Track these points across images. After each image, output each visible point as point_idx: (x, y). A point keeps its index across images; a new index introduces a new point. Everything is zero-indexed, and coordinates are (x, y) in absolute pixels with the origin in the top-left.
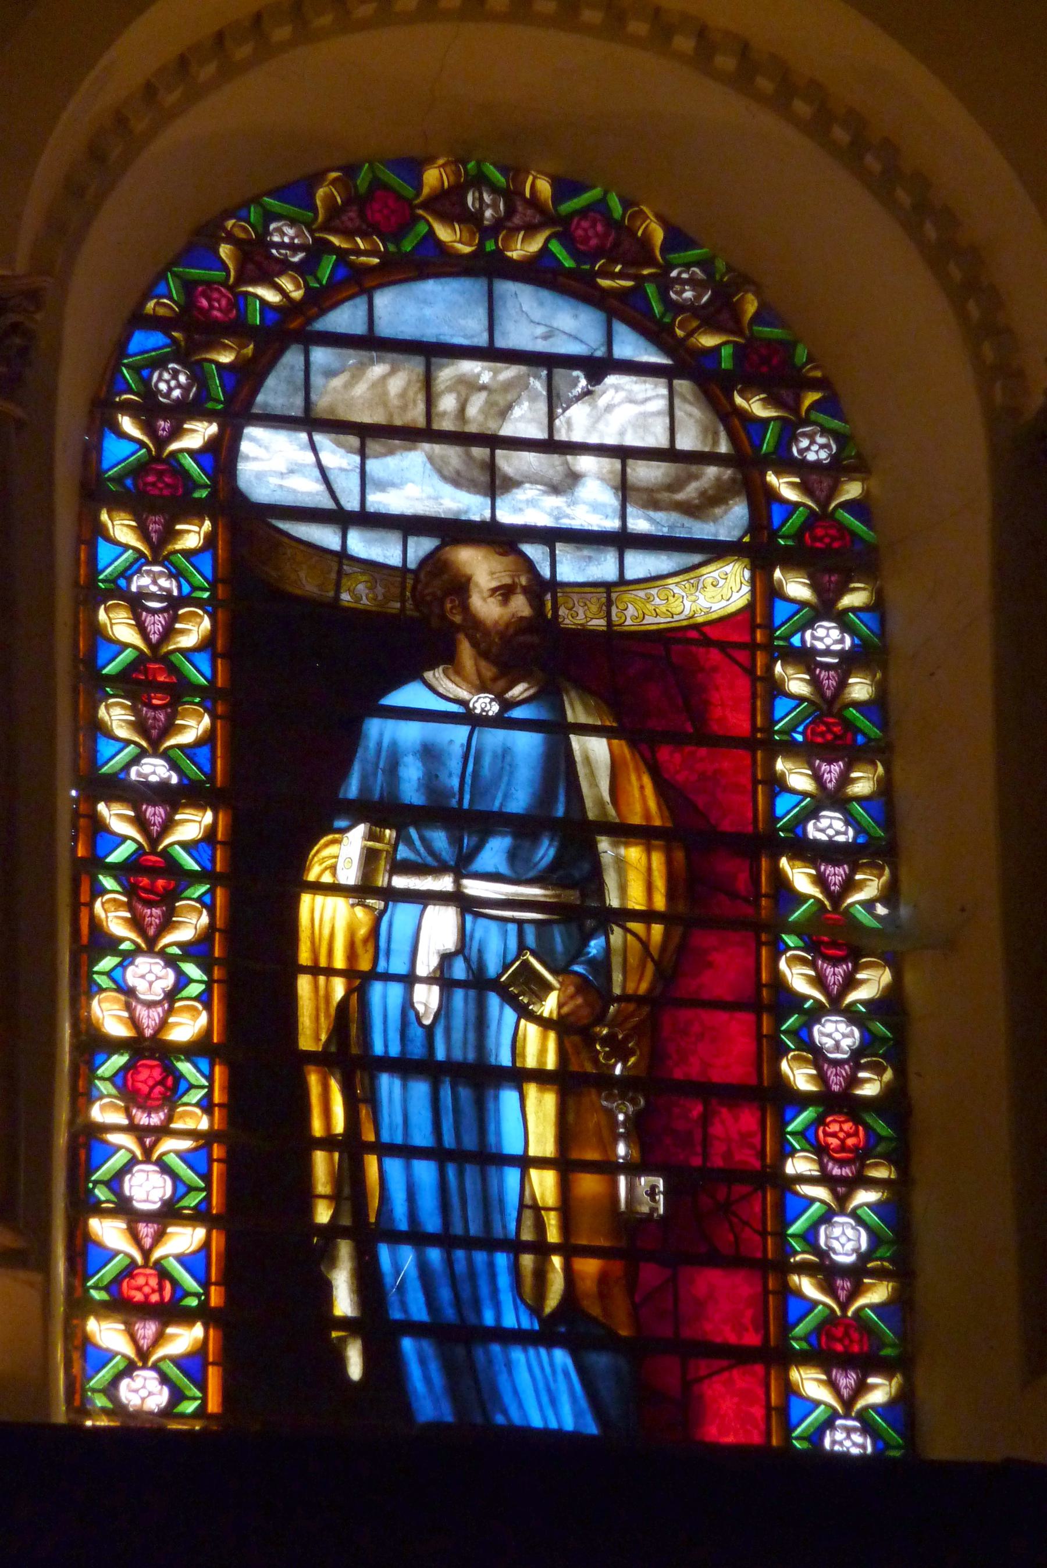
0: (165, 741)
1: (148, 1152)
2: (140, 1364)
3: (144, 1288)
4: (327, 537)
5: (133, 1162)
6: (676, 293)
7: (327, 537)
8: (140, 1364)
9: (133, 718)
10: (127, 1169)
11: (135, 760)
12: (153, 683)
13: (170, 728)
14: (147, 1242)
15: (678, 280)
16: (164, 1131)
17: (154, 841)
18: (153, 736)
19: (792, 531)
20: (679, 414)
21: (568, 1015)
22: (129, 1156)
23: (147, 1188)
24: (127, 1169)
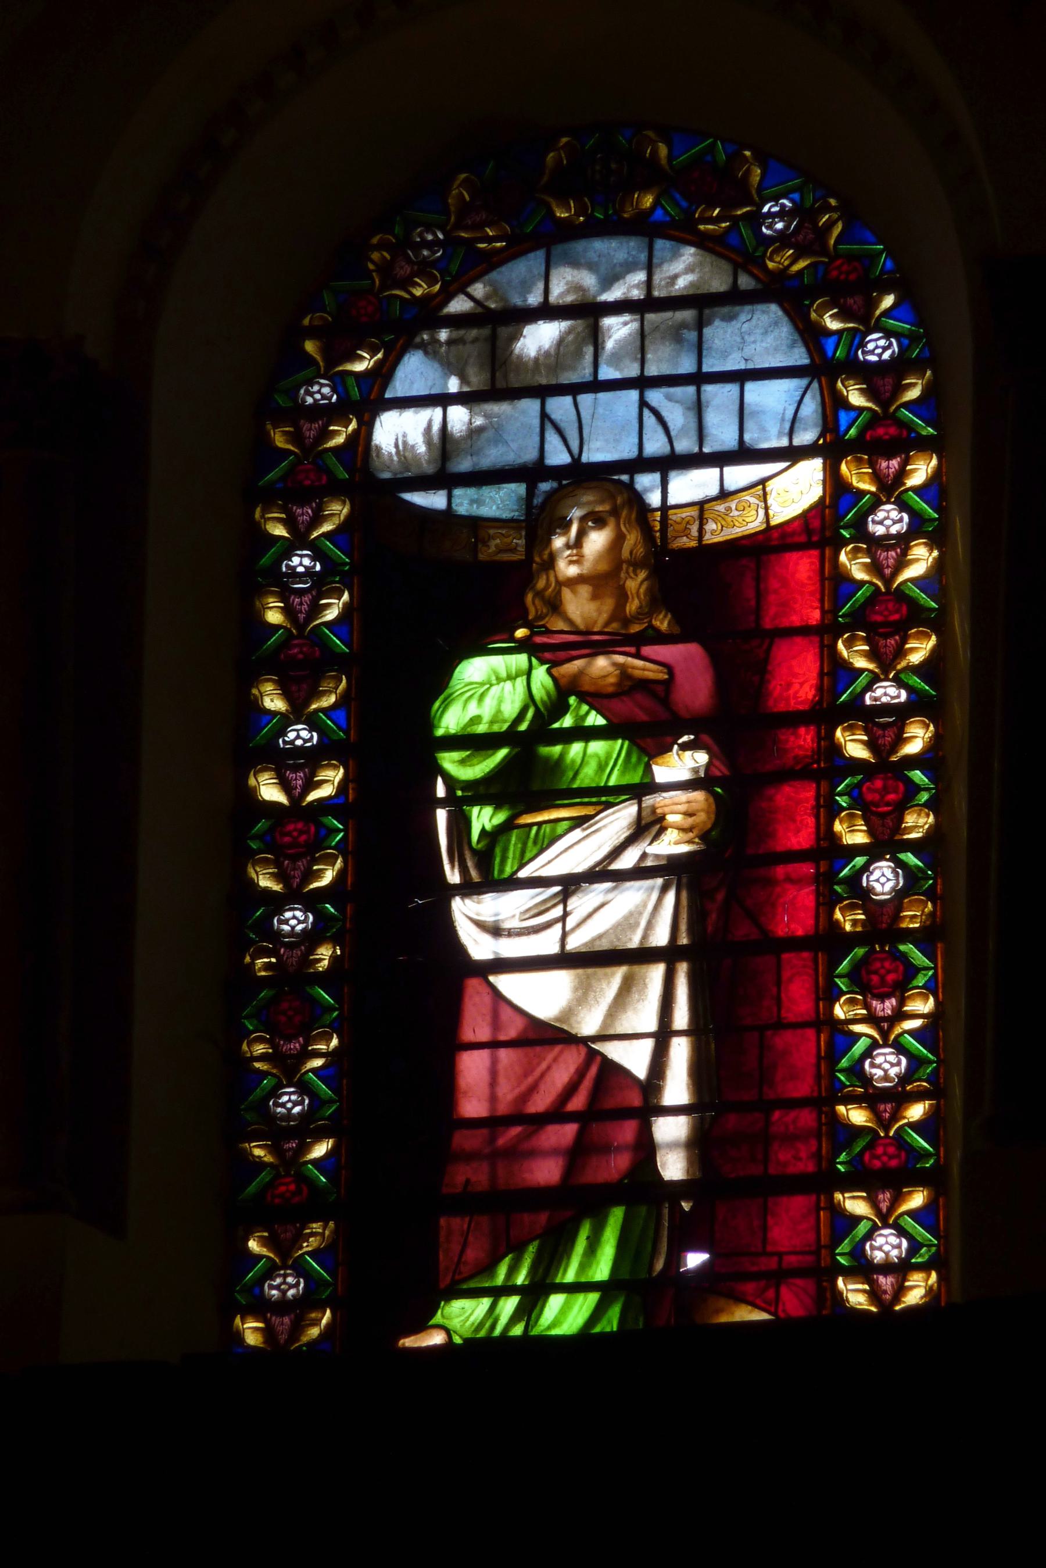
0: (900, 1206)
1: (885, 1034)
2: (882, 677)
3: (884, 1159)
4: (435, 500)
5: (875, 1045)
6: (767, 228)
7: (435, 500)
8: (882, 677)
9: (867, 648)
10: (868, 1053)
11: (869, 687)
12: (883, 788)
13: (901, 652)
14: (884, 1206)
15: (770, 214)
16: (901, 1015)
17: (888, 581)
18: (887, 661)
19: (754, 243)
20: (734, 363)
21: (544, 550)
22: (870, 1224)
23: (886, 1246)
24: (868, 1053)
